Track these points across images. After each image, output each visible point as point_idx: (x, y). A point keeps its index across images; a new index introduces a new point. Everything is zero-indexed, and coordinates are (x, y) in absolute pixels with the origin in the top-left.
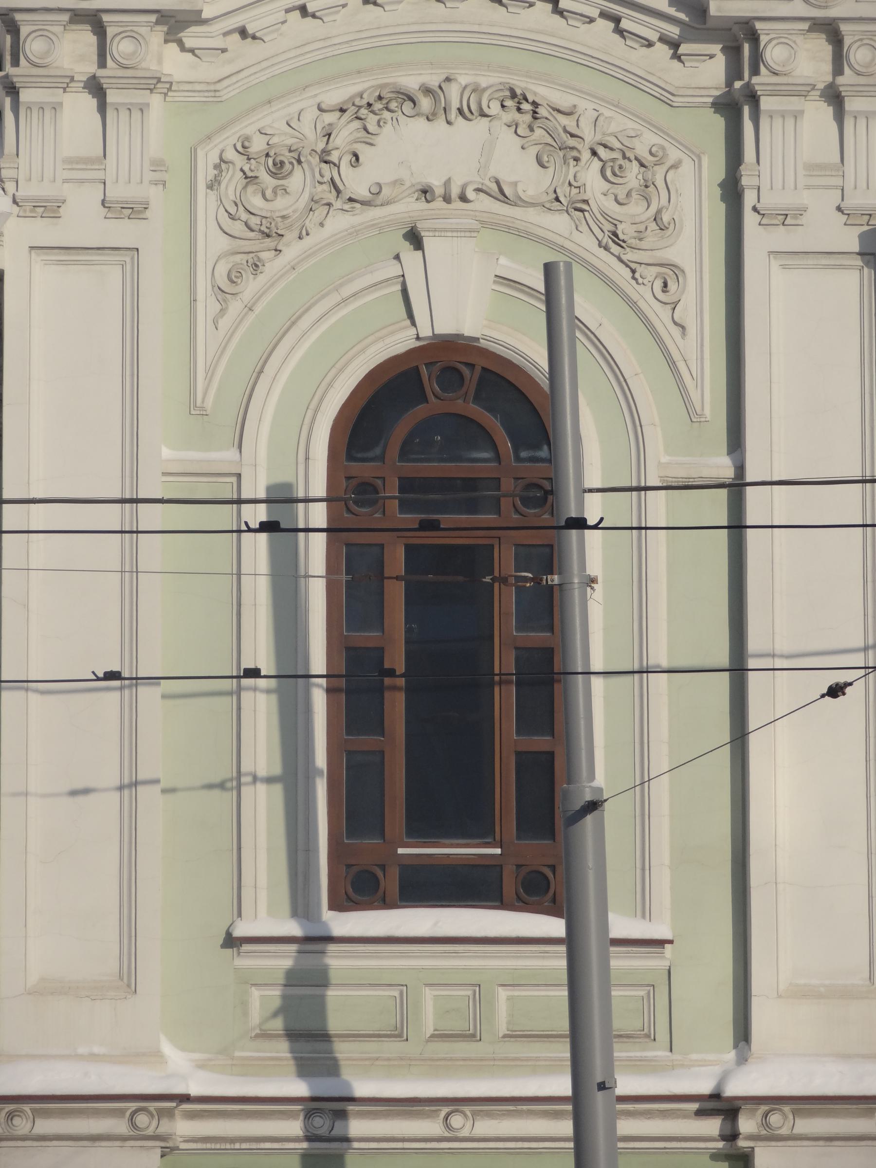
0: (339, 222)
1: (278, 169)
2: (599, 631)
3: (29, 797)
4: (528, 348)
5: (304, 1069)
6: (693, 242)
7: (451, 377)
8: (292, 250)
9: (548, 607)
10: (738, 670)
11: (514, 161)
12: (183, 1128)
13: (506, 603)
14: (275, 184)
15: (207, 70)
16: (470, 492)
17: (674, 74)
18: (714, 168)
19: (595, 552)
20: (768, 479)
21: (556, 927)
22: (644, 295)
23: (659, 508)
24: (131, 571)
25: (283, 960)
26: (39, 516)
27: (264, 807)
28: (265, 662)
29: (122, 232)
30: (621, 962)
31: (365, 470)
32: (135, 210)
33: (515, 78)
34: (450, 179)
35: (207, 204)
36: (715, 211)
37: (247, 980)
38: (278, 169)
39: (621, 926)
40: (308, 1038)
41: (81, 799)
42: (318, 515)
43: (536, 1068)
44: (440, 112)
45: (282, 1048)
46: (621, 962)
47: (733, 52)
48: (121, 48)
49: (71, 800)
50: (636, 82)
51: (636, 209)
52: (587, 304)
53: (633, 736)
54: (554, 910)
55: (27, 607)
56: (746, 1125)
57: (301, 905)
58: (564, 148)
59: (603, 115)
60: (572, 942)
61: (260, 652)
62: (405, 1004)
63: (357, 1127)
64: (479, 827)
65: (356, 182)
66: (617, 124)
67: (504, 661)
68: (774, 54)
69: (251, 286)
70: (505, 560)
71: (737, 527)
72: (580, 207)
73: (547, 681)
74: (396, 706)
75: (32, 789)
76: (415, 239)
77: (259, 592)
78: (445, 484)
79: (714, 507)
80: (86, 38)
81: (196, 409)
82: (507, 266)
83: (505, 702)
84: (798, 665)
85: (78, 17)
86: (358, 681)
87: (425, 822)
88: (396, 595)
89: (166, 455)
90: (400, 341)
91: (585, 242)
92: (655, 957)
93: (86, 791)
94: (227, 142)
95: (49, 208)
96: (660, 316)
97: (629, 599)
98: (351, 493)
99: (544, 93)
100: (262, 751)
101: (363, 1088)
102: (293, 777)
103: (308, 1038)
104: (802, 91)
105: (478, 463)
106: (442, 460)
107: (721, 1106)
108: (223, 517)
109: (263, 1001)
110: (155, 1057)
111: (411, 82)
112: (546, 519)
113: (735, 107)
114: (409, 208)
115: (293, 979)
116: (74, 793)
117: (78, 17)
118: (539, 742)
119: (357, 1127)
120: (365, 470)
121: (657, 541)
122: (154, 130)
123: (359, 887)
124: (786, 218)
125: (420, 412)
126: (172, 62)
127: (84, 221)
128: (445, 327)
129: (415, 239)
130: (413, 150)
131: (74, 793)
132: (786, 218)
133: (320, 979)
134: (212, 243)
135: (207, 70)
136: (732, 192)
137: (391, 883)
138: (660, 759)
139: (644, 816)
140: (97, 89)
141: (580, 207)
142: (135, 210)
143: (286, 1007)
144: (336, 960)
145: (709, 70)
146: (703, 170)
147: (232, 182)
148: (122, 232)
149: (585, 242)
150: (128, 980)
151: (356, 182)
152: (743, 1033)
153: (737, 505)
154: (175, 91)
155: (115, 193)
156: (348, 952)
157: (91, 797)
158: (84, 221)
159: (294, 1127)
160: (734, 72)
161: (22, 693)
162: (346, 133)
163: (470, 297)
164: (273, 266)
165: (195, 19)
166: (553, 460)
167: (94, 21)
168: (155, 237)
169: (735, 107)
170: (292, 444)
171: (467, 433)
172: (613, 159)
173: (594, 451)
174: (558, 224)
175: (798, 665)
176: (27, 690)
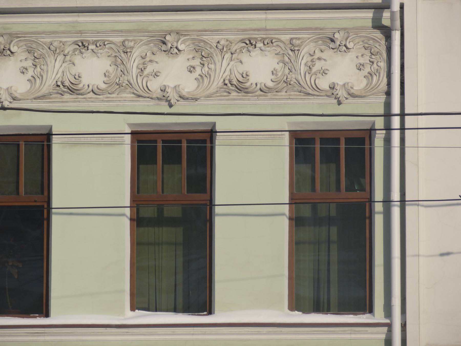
3: (420, 257)
20: (407, 144)
26: (423, 121)
33: (57, 35)
34: (74, 65)
41: (445, 258)
49: (440, 258)
55: (417, 165)
75: (421, 253)
92: (40, 335)
93: (448, 254)
116: (442, 255)
131: (442, 255)
156: (67, 333)
157: (451, 257)
161: (416, 207)
176: (418, 205)
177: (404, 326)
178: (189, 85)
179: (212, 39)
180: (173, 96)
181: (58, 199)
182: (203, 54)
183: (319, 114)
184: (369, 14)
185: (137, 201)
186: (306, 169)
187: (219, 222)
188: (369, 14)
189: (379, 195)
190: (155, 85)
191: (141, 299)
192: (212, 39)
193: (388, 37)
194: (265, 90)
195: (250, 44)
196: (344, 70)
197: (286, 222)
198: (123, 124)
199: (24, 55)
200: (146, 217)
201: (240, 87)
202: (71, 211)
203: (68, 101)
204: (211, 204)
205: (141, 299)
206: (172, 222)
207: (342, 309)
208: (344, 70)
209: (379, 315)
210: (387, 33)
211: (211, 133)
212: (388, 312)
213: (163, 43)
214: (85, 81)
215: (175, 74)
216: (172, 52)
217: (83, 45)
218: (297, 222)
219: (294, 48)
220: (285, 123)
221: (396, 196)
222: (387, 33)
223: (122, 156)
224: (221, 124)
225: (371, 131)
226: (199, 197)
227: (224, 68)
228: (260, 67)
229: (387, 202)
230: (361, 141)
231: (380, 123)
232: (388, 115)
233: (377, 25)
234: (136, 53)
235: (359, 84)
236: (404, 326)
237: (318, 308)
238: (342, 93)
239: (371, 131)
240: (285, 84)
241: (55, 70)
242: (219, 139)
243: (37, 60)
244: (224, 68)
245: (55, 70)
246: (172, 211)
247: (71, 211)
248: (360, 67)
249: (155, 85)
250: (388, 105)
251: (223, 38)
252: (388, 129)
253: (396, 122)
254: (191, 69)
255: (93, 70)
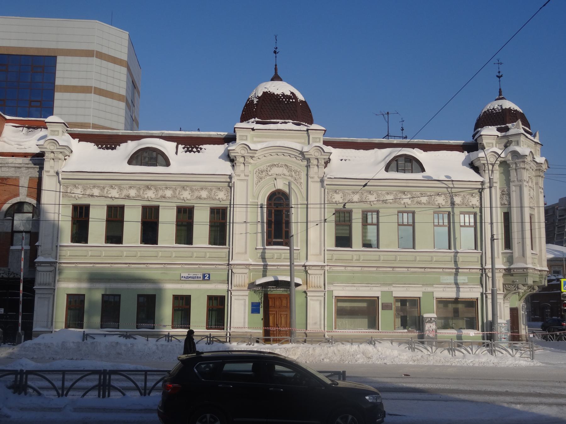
0: (268, 177)
1: (262, 172)
2: (293, 219)
4: (287, 190)
5: (263, 262)
6: (303, 180)
7: (279, 193)
8: (263, 180)
9: (288, 216)
10: (307, 222)
11: (286, 172)
12: (251, 267)
13: (284, 216)
14: (262, 173)
15: (255, 162)
16: (281, 205)
17: (302, 163)
18: (306, 173)
19: (293, 211)
21: (288, 248)
22: (298, 185)
23: (299, 206)
24: (247, 212)
25: (261, 251)
26: (238, 206)
27: (260, 235)
28: (260, 221)
29: (246, 178)
30: (295, 252)
31: (270, 202)
32: (248, 176)
35: (255, 175)
36: (305, 177)
37: (258, 253)
38: (262, 172)
39: (295, 248)
40: (263, 258)
42: (266, 206)
43: (286, 262)
44: (278, 166)
45: (261, 260)
46: (295, 252)
47: (308, 161)
48: (246, 160)
50: (298, 164)
51: (298, 177)
52: (293, 186)
53: (296, 229)
54: (288, 246)
56: (307, 268)
57: (263, 245)
58: (291, 170)
59: (294, 167)
60: (290, 250)
61: (259, 220)
62: (273, 255)
63: (268, 267)
64: (281, 238)
65: (270, 173)
66: (296, 168)
67: (284, 221)
68: (312, 161)
69: (259, 184)
70: (284, 211)
71: (307, 208)
72: (292, 176)
73: (288, 223)
74: (273, 226)
76: (276, 179)
77: (259, 214)
78: (278, 204)
79: (305, 206)
80: (243, 159)
81: (253, 196)
82: (285, 182)
83: (284, 225)
84: (313, 222)
85: (242, 156)
86: (269, 223)
87: (275, 238)
88: (273, 215)
89: (250, 200)
90: (274, 189)
91: (292, 180)
94: (257, 169)
95: (239, 176)
96: (300, 187)
97: (296, 215)
98: (269, 205)
99: (288, 165)
100: (259, 230)
101: (269, 264)
102: (262, 233)
103: (263, 258)
104: (314, 165)
105: (281, 202)
106: (181, 328)
107: (305, 266)
108: (256, 206)
109: (259, 255)
110: (248, 260)
111: (275, 164)
112: (288, 207)
113: (308, 167)
114: (275, 176)
115: (262, 253)
117: (242, 156)
118: (287, 230)
119: (268, 267)
120: (270, 202)
121: (299, 224)
122: (250, 168)
123: (269, 244)
124: (312, 178)
125: (275, 197)
126: (251, 161)
127: (242, 177)
128: (278, 188)
129: (276, 179)
130: (275, 170)
132: (312, 178)
133: (265, 253)
134: (255, 179)
135: (255, 162)
136: (307, 175)
137: (272, 243)
138: (299, 231)
139: (297, 237)
140: (244, 164)
141: (292, 176)
142: (248, 176)
143: (261, 256)
144: (266, 251)
145: (305, 163)
146: (466, 399)
147: (257, 173)
148: (246, 178)
149: (292, 180)
150: (246, 253)
151: (270, 173)
152: (307, 259)
153: (307, 206)
154: (477, 189)
155: (246, 174)
158: (242, 177)
159: (262, 267)
160: (308, 163)
162: (269, 169)
163: (281, 185)
164: (261, 182)
165: (254, 157)
166: (289, 201)
167: (244, 157)
168: (249, 178)
169: (308, 167)
170: (263, 199)
171: (280, 199)
172: (296, 172)
173: (293, 201)
174: (290, 178)
175: (313, 222)
177: (485, 253)
178: (189, 197)
179: (194, 188)
180: (186, 200)
181: (161, 219)
182: (192, 190)
183: (216, 204)
184: (227, 184)
185: (177, 221)
186: (213, 215)
187: (194, 226)
188: (227, 184)
189: (228, 221)
190: (182, 197)
191: (178, 241)
192: (194, 188)
193: (231, 189)
194: (205, 199)
195: (202, 189)
196: (222, 195)
197: (208, 226)
198: (175, 205)
199: (341, 194)
200: (179, 224)
201: (200, 198)
202: (163, 223)
203: (419, 206)
204: (193, 222)
205: (178, 241)
206: (184, 226)
207: (219, 245)
208: (222, 195)
209: (227, 246)
210: (231, 188)
211: (193, 207)
212: (229, 246)
213: (183, 188)
214: (167, 195)
215: (186, 195)
216: (185, 190)
217: (167, 188)
218: (211, 226)
219: (211, 190)
220: (209, 206)
221: (232, 221)
222: (231, 188)
223: (174, 212)
224: (195, 205)
225: (227, 208)
226: (190, 221)
227: (196, 194)
228: (204, 194)
229: (230, 222)
230: (225, 210)
231: (229, 206)
232: (230, 205)
233: (229, 186)
234: (178, 190)
235: (225, 198)
236: (485, 253)
237: (215, 244)
238: (221, 200)
239: (227, 208)
240: (209, 198)
241: (161, 193)
242: (195, 208)
243: (157, 191)
244: (196, 194)
245: (161, 193)
246: (184, 223)
247: (163, 223)
248: (118, 192)
249: (182, 197)
250: (230, 202)
251: (196, 187)
252: (230, 207)
253: (232, 206)
254: (190, 194)
255: (169, 193)
